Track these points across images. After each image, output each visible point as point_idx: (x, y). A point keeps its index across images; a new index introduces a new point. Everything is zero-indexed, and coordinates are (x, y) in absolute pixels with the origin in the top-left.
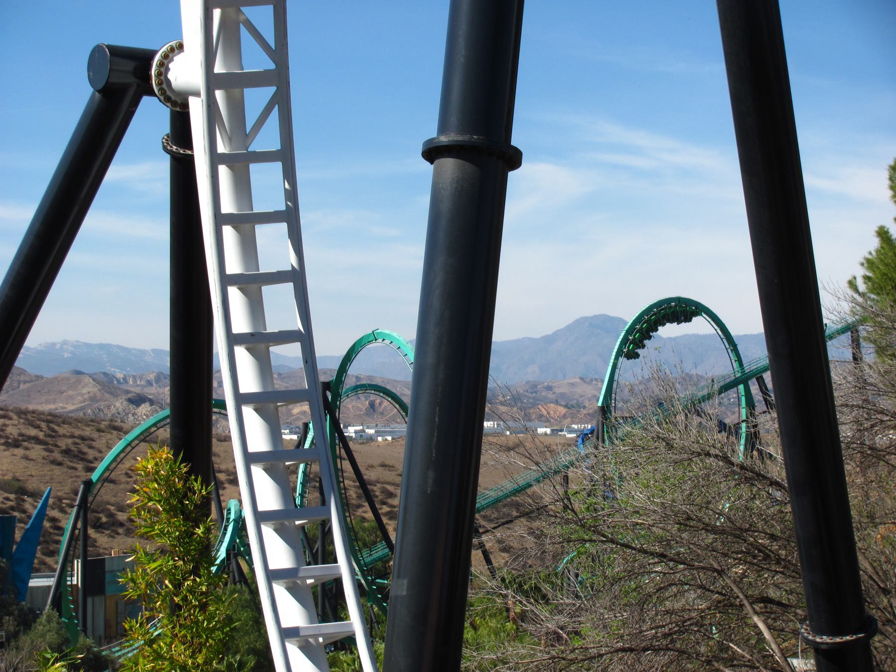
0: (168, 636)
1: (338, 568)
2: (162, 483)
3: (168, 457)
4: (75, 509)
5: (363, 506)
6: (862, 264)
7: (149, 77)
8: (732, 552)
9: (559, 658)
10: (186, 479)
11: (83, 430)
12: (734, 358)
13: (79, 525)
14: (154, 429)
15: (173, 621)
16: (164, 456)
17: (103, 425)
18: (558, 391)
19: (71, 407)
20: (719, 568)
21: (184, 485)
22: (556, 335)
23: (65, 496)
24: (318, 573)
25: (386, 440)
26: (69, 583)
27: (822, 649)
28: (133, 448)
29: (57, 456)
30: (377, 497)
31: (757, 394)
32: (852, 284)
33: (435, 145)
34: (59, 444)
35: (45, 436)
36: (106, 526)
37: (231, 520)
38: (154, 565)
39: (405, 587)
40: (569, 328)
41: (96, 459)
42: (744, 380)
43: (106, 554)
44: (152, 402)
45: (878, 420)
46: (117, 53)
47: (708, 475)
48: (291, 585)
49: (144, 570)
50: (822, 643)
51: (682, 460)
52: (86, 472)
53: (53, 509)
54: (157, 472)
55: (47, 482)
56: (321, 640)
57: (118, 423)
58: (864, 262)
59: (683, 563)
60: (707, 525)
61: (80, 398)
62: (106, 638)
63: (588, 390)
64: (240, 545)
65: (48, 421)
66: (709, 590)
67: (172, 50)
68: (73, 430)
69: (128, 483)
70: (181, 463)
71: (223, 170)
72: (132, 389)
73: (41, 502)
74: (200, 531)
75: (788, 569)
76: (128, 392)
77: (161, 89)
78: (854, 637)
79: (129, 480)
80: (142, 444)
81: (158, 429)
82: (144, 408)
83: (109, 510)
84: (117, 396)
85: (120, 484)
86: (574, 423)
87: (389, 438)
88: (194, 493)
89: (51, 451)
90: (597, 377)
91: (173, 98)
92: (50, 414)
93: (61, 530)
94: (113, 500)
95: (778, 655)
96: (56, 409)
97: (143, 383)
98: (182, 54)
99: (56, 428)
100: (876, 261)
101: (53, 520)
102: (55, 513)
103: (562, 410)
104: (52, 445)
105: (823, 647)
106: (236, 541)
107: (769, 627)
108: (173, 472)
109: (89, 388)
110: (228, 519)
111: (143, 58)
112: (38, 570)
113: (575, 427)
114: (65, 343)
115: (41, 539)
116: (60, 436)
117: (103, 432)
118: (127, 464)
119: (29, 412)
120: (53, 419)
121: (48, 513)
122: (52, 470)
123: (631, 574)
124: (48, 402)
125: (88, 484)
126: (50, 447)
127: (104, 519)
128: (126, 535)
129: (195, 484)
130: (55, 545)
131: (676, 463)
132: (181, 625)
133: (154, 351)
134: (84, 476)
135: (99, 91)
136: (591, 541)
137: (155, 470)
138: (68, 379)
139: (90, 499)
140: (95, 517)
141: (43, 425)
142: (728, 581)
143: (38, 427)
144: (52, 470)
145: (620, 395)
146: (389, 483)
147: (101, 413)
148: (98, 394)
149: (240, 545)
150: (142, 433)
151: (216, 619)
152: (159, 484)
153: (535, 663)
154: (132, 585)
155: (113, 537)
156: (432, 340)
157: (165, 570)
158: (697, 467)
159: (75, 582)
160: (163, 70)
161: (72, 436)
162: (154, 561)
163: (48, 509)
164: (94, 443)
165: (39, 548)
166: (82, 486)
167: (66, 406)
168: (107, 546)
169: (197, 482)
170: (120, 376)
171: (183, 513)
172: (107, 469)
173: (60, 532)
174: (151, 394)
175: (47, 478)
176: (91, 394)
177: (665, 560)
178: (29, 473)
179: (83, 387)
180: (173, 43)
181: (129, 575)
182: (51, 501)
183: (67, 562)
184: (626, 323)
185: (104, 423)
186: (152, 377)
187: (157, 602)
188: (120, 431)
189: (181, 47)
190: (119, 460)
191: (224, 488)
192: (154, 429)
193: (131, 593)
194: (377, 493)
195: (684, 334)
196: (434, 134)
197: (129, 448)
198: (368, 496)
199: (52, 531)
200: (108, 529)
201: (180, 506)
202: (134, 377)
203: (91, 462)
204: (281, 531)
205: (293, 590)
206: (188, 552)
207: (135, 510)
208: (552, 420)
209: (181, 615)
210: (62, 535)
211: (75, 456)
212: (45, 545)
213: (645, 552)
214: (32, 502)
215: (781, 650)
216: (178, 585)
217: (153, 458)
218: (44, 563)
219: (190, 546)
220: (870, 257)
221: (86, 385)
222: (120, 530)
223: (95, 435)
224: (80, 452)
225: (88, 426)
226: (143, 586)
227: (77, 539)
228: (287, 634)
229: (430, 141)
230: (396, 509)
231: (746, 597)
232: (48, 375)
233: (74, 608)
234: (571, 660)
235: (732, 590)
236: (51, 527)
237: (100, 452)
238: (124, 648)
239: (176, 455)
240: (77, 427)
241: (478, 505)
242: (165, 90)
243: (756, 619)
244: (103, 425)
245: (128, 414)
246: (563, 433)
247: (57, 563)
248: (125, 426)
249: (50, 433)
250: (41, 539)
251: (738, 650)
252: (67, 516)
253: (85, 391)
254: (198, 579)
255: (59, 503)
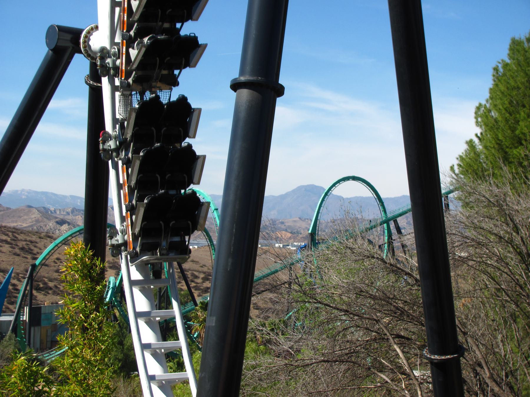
0: (81, 345)
1: (173, 312)
2: (79, 261)
3: (82, 247)
4: (26, 280)
5: (181, 283)
6: (457, 159)
7: (79, 44)
8: (384, 310)
9: (289, 364)
10: (92, 258)
11: (32, 237)
12: (382, 209)
13: (28, 288)
14: (69, 238)
15: (84, 336)
16: (80, 247)
17: (43, 235)
18: (287, 224)
19: (25, 225)
20: (377, 319)
21: (91, 262)
22: (286, 195)
23: (21, 272)
24: (162, 314)
25: (195, 248)
26: (21, 319)
27: (435, 363)
28: (59, 247)
29: (17, 251)
30: (189, 278)
31: (393, 230)
32: (452, 168)
33: (237, 82)
34: (18, 244)
35: (11, 240)
36: (42, 289)
37: (110, 287)
38: (74, 305)
39: (214, 321)
40: (294, 191)
41: (38, 253)
42: (387, 221)
43: (42, 304)
44: (69, 224)
45: (463, 242)
46: (62, 30)
47: (372, 268)
48: (148, 320)
49: (68, 308)
50: (435, 359)
51: (359, 260)
52: (33, 260)
53: (14, 279)
54: (76, 255)
55: (11, 265)
56: (163, 350)
57: (51, 234)
58: (458, 157)
59: (358, 316)
60: (371, 295)
61: (30, 220)
62: (41, 349)
63: (303, 225)
64: (115, 301)
65: (13, 232)
66: (371, 330)
67: (92, 29)
68: (26, 237)
69: (55, 266)
70: (89, 250)
71: (118, 94)
72: (58, 216)
73: (8, 275)
74: (98, 288)
75: (414, 320)
76: (56, 218)
77: (85, 50)
78: (452, 356)
79: (56, 265)
80: (63, 245)
81: (73, 238)
82: (65, 227)
83: (44, 281)
84: (50, 220)
85: (51, 267)
86: (295, 242)
87: (196, 247)
88: (97, 267)
89: (14, 248)
90: (308, 218)
91: (92, 55)
92: (14, 228)
93: (18, 291)
94: (47, 275)
95: (407, 366)
96: (17, 226)
97: (64, 213)
98: (97, 31)
99: (17, 235)
100: (464, 157)
101: (14, 285)
102: (15, 281)
103: (289, 235)
104: (14, 245)
105: (435, 361)
106: (112, 299)
107: (403, 352)
108: (85, 255)
109: (36, 215)
110: (109, 287)
111: (76, 33)
112: (5, 312)
113: (296, 244)
114: (23, 190)
115: (7, 295)
116: (19, 240)
117: (42, 238)
118: (55, 256)
119: (3, 227)
120: (15, 231)
121: (11, 281)
122: (14, 258)
123: (329, 321)
124: (13, 222)
125: (34, 266)
126: (13, 246)
127: (41, 286)
128: (53, 294)
129: (97, 261)
130: (14, 299)
131: (356, 261)
132: (88, 339)
133: (71, 196)
134: (31, 262)
135: (52, 50)
136: (309, 302)
137: (75, 254)
138: (24, 210)
139: (34, 274)
140: (37, 284)
141: (10, 234)
142: (381, 326)
143: (7, 235)
144: (14, 258)
145: (321, 226)
146: (195, 271)
147: (41, 229)
148: (40, 218)
149: (115, 301)
150: (64, 240)
151: (108, 335)
152: (77, 262)
153: (276, 367)
154: (61, 316)
155: (46, 295)
156: (233, 188)
157: (80, 308)
158: (367, 263)
159: (25, 319)
160: (87, 40)
161: (26, 241)
162: (74, 303)
163: (11, 279)
164: (37, 245)
165: (6, 300)
166: (30, 267)
167: (23, 224)
168: (42, 300)
169: (98, 261)
170: (52, 209)
171: (90, 278)
172: (44, 258)
173: (17, 292)
174: (68, 219)
175: (11, 262)
176: (36, 218)
177: (348, 314)
178: (2, 260)
179: (32, 215)
180: (93, 26)
181: (61, 311)
182: (13, 275)
183: (21, 307)
184: (325, 190)
185: (43, 234)
186: (69, 210)
187: (76, 326)
188: (52, 238)
189: (97, 28)
190: (51, 254)
191: (107, 271)
192: (69, 238)
193: (61, 321)
194: (189, 276)
195: (354, 196)
196: (237, 76)
197: (56, 248)
198: (185, 278)
199: (13, 291)
200: (43, 291)
201: (89, 274)
202: (60, 210)
203: (35, 254)
204: (143, 291)
205: (149, 323)
206: (93, 299)
207: (64, 276)
208: (283, 240)
209: (88, 333)
210: (19, 293)
211: (27, 251)
212: (9, 298)
213: (338, 309)
214: (3, 275)
215: (409, 364)
216: (87, 317)
217: (74, 248)
218: (8, 308)
219: (94, 295)
220: (461, 154)
221: (34, 213)
222: (50, 292)
223: (38, 240)
224: (30, 249)
225: (34, 235)
226: (68, 317)
227: (27, 296)
228: (145, 347)
229: (236, 79)
230: (199, 285)
231: (391, 335)
232: (13, 207)
233: (24, 333)
234: (296, 366)
235: (383, 330)
236: (13, 289)
237: (40, 249)
238: (51, 355)
239: (86, 245)
240: (28, 235)
241: (255, 278)
242: (88, 51)
243: (395, 347)
244: (43, 235)
245: (55, 230)
246: (289, 247)
247: (15, 308)
248: (55, 236)
249: (14, 238)
250: (7, 295)
251: (386, 363)
252: (21, 283)
253: (33, 216)
254: (98, 314)
255: (17, 276)
